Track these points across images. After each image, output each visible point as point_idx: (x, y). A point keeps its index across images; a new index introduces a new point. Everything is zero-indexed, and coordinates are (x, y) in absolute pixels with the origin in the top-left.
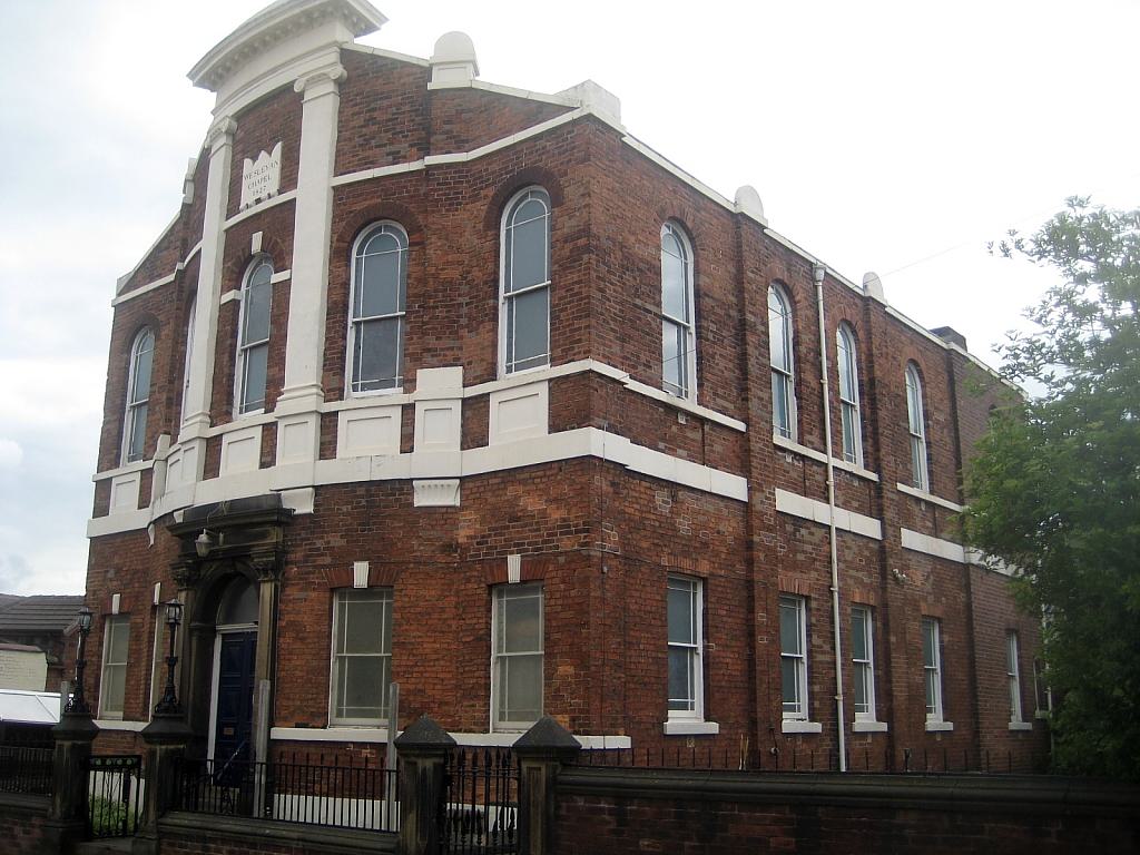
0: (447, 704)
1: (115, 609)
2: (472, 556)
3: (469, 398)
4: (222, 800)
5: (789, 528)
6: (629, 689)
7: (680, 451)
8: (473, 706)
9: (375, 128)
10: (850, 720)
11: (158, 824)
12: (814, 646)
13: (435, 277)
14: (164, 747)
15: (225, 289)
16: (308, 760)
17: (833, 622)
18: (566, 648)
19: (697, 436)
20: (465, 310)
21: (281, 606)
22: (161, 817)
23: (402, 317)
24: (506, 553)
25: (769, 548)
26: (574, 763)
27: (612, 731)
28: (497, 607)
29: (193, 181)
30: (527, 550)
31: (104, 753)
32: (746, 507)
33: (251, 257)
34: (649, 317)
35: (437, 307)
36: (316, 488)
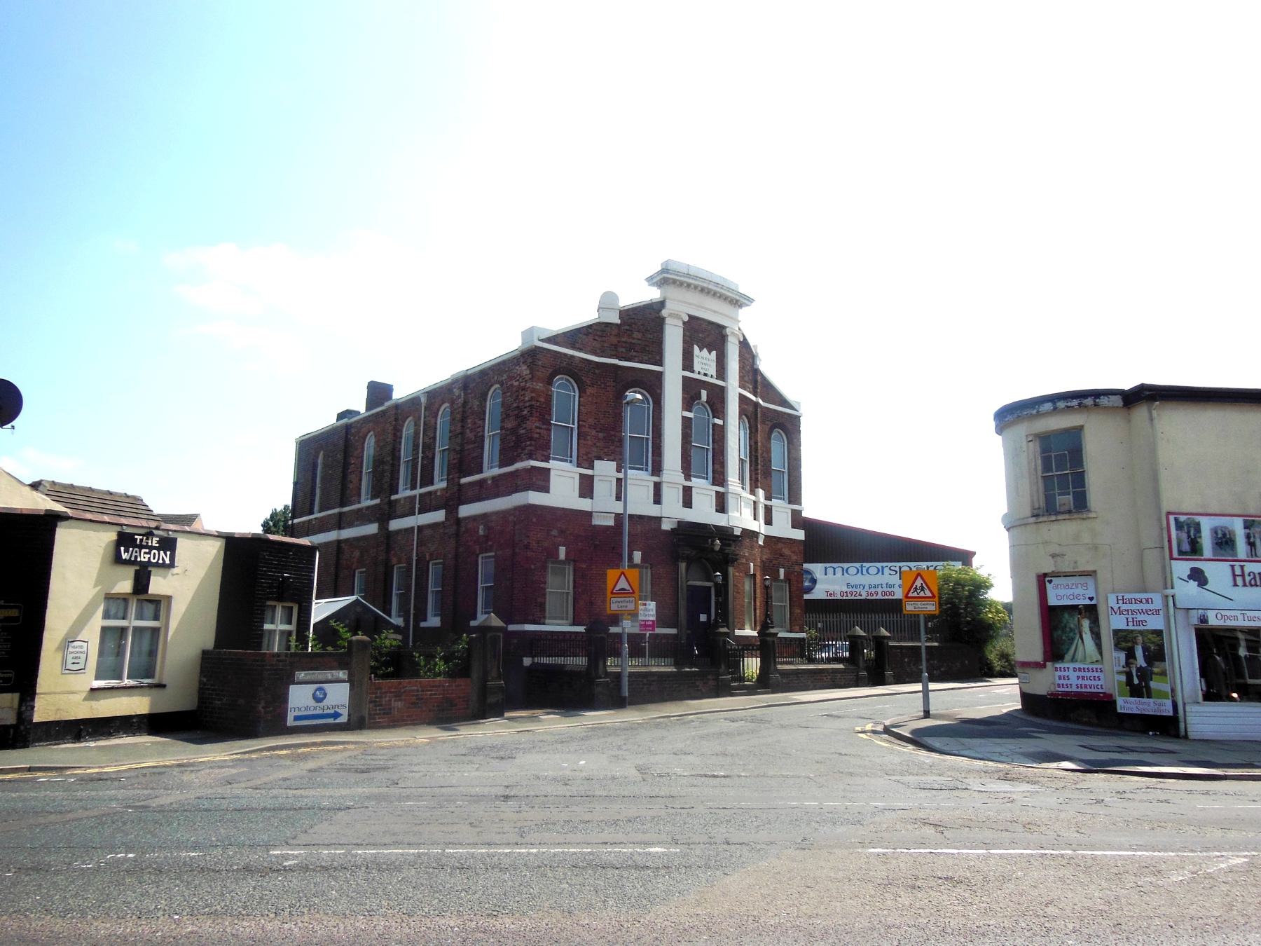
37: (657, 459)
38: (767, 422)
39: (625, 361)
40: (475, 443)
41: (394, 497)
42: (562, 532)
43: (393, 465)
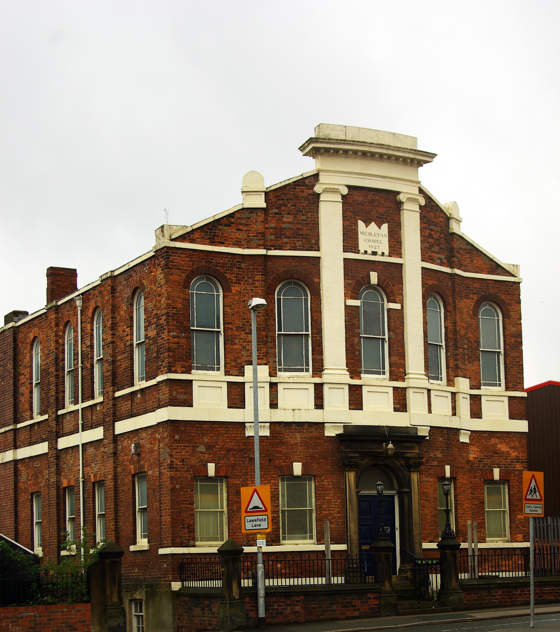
2: (476, 467)
8: (481, 531)
24: (492, 467)
30: (502, 467)
37: (318, 357)
38: (471, 296)
39: (275, 249)
40: (124, 353)
41: (60, 412)
42: (209, 447)
43: (57, 376)
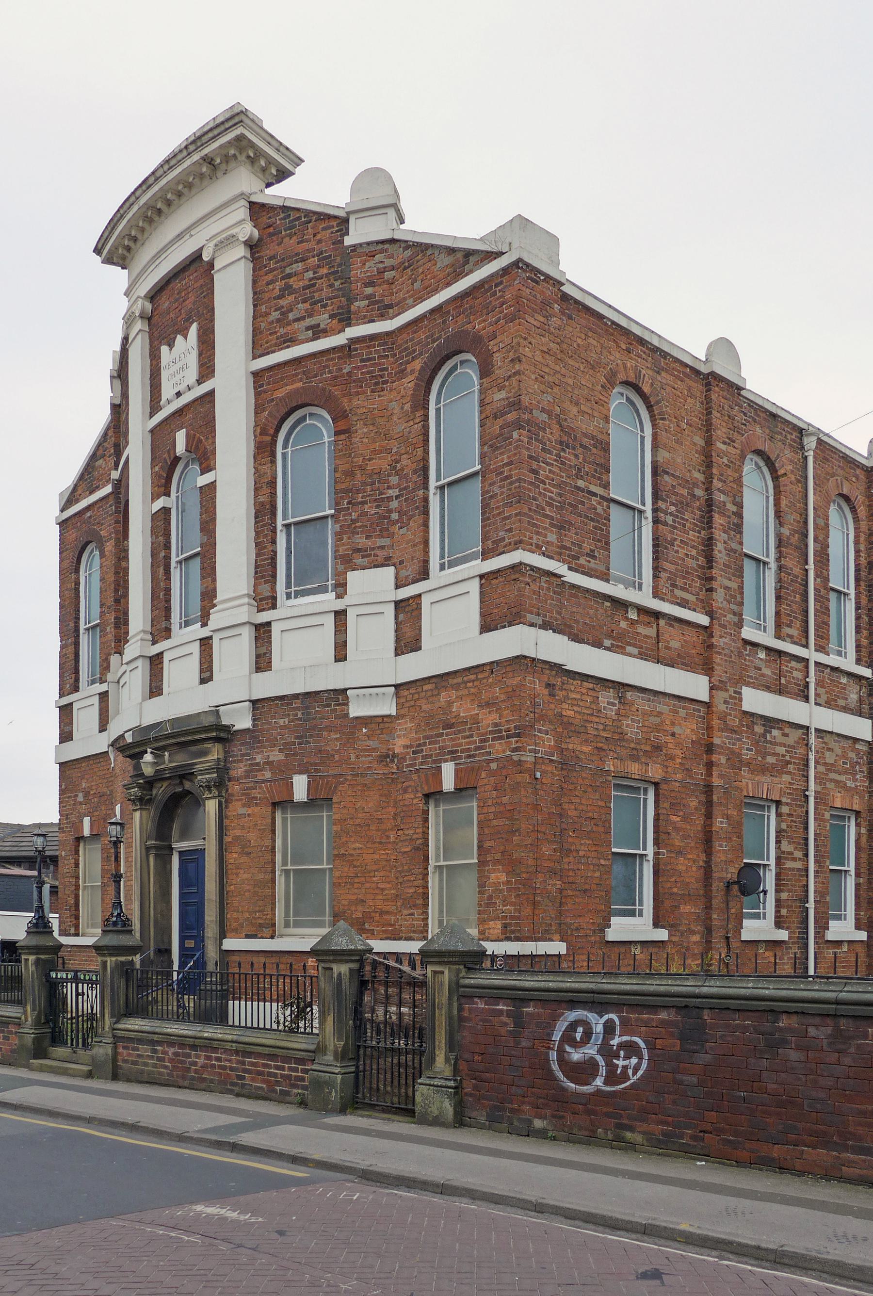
0: (387, 913)
1: (87, 832)
3: (402, 601)
4: (179, 1007)
5: (759, 729)
6: (566, 897)
7: (629, 649)
8: (412, 914)
9: (291, 298)
10: (822, 927)
11: (114, 1029)
12: (783, 852)
13: (362, 468)
14: (114, 959)
15: (155, 497)
16: (265, 968)
17: (806, 828)
18: (498, 856)
19: (651, 632)
20: (394, 504)
21: (226, 822)
22: (115, 1023)
23: (332, 516)
24: (440, 761)
25: (732, 752)
26: (478, 967)
27: (545, 937)
28: (435, 815)
29: (119, 376)
30: (460, 758)
31: (88, 968)
32: (708, 705)
33: (177, 459)
34: (594, 501)
35: (365, 503)
36: (254, 702)
